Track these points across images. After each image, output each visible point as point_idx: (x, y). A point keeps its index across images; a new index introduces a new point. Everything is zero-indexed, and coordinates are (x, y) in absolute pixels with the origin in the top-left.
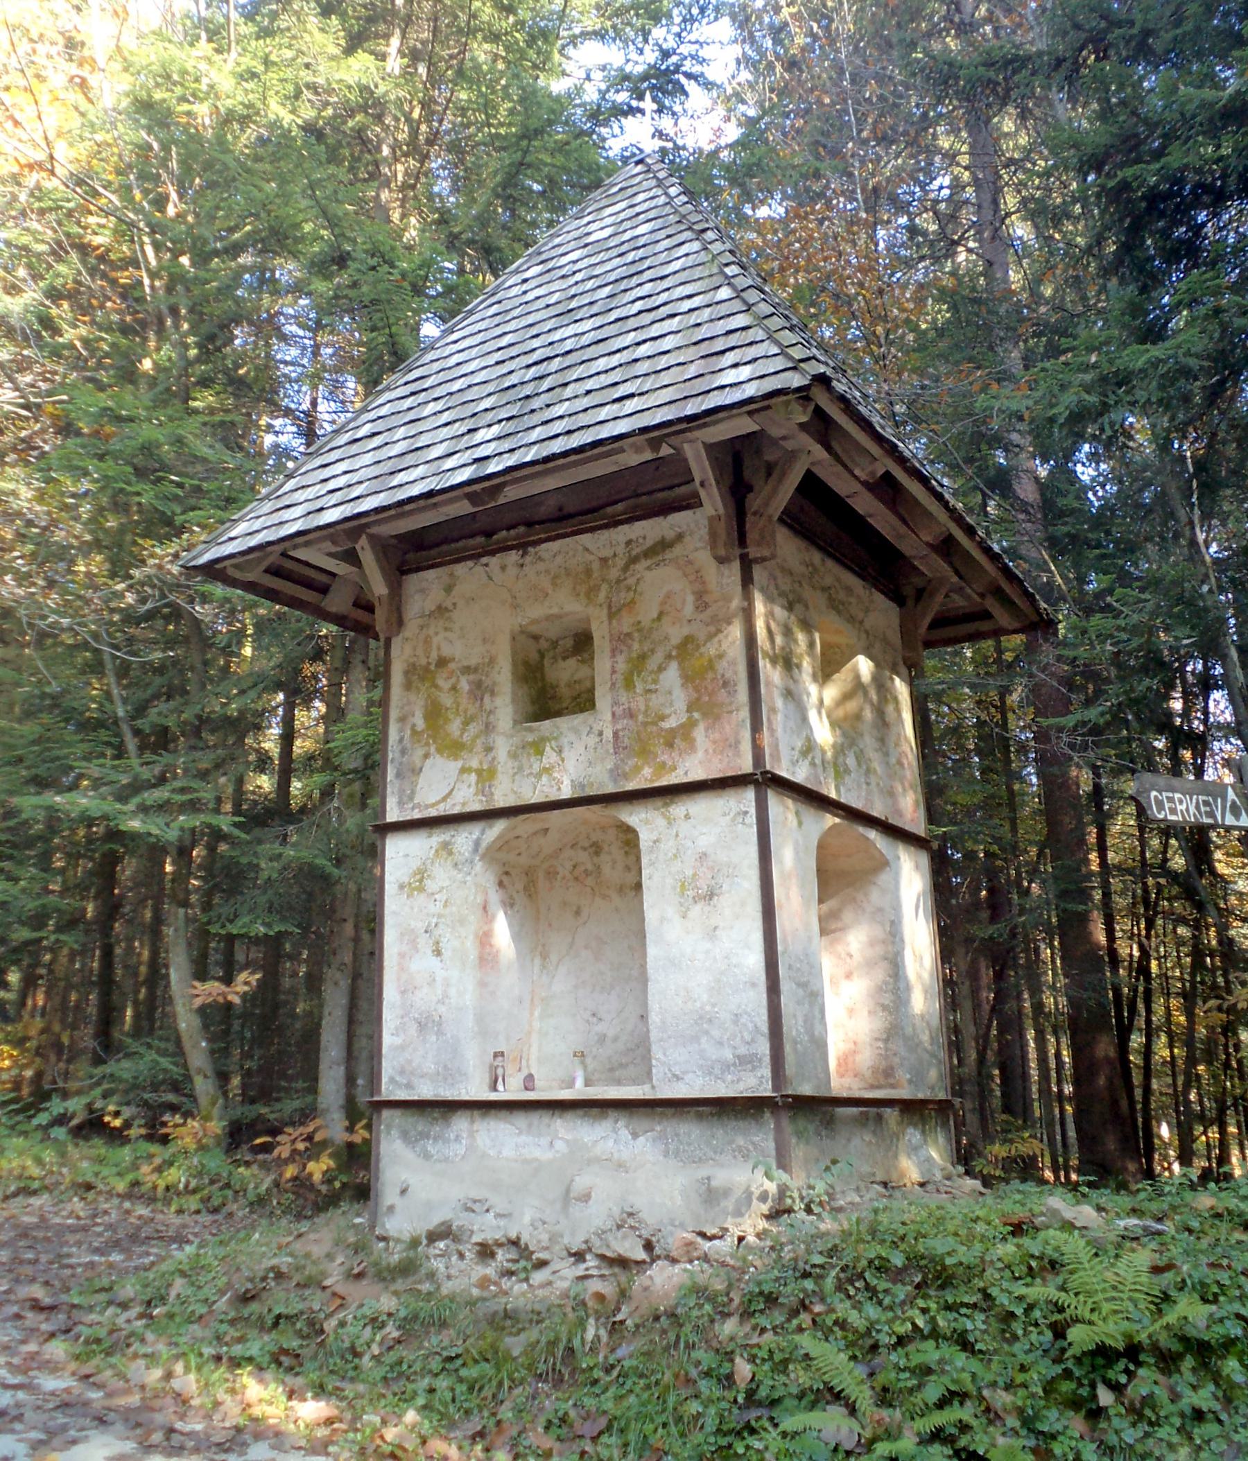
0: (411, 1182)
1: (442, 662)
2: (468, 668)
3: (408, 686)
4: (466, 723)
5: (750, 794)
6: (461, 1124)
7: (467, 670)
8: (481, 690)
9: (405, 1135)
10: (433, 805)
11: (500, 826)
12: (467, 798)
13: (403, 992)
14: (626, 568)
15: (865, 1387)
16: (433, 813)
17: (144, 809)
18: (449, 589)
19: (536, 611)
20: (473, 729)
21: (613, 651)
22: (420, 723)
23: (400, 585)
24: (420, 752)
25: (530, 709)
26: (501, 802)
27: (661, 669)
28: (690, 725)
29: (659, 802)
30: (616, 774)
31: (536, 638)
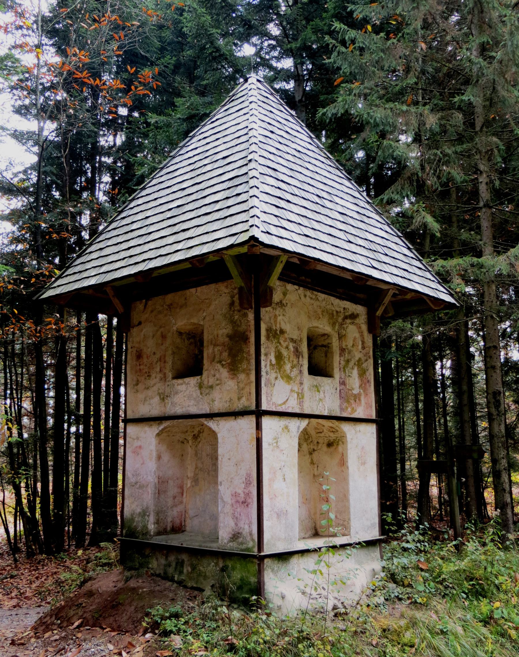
0: (284, 592)
1: (282, 332)
2: (292, 339)
3: (268, 338)
4: (292, 367)
7: (292, 340)
9: (273, 570)
10: (280, 405)
12: (293, 407)
13: (271, 499)
15: (85, 646)
19: (315, 324)
21: (340, 354)
22: (274, 361)
26: (307, 411)
27: (353, 369)
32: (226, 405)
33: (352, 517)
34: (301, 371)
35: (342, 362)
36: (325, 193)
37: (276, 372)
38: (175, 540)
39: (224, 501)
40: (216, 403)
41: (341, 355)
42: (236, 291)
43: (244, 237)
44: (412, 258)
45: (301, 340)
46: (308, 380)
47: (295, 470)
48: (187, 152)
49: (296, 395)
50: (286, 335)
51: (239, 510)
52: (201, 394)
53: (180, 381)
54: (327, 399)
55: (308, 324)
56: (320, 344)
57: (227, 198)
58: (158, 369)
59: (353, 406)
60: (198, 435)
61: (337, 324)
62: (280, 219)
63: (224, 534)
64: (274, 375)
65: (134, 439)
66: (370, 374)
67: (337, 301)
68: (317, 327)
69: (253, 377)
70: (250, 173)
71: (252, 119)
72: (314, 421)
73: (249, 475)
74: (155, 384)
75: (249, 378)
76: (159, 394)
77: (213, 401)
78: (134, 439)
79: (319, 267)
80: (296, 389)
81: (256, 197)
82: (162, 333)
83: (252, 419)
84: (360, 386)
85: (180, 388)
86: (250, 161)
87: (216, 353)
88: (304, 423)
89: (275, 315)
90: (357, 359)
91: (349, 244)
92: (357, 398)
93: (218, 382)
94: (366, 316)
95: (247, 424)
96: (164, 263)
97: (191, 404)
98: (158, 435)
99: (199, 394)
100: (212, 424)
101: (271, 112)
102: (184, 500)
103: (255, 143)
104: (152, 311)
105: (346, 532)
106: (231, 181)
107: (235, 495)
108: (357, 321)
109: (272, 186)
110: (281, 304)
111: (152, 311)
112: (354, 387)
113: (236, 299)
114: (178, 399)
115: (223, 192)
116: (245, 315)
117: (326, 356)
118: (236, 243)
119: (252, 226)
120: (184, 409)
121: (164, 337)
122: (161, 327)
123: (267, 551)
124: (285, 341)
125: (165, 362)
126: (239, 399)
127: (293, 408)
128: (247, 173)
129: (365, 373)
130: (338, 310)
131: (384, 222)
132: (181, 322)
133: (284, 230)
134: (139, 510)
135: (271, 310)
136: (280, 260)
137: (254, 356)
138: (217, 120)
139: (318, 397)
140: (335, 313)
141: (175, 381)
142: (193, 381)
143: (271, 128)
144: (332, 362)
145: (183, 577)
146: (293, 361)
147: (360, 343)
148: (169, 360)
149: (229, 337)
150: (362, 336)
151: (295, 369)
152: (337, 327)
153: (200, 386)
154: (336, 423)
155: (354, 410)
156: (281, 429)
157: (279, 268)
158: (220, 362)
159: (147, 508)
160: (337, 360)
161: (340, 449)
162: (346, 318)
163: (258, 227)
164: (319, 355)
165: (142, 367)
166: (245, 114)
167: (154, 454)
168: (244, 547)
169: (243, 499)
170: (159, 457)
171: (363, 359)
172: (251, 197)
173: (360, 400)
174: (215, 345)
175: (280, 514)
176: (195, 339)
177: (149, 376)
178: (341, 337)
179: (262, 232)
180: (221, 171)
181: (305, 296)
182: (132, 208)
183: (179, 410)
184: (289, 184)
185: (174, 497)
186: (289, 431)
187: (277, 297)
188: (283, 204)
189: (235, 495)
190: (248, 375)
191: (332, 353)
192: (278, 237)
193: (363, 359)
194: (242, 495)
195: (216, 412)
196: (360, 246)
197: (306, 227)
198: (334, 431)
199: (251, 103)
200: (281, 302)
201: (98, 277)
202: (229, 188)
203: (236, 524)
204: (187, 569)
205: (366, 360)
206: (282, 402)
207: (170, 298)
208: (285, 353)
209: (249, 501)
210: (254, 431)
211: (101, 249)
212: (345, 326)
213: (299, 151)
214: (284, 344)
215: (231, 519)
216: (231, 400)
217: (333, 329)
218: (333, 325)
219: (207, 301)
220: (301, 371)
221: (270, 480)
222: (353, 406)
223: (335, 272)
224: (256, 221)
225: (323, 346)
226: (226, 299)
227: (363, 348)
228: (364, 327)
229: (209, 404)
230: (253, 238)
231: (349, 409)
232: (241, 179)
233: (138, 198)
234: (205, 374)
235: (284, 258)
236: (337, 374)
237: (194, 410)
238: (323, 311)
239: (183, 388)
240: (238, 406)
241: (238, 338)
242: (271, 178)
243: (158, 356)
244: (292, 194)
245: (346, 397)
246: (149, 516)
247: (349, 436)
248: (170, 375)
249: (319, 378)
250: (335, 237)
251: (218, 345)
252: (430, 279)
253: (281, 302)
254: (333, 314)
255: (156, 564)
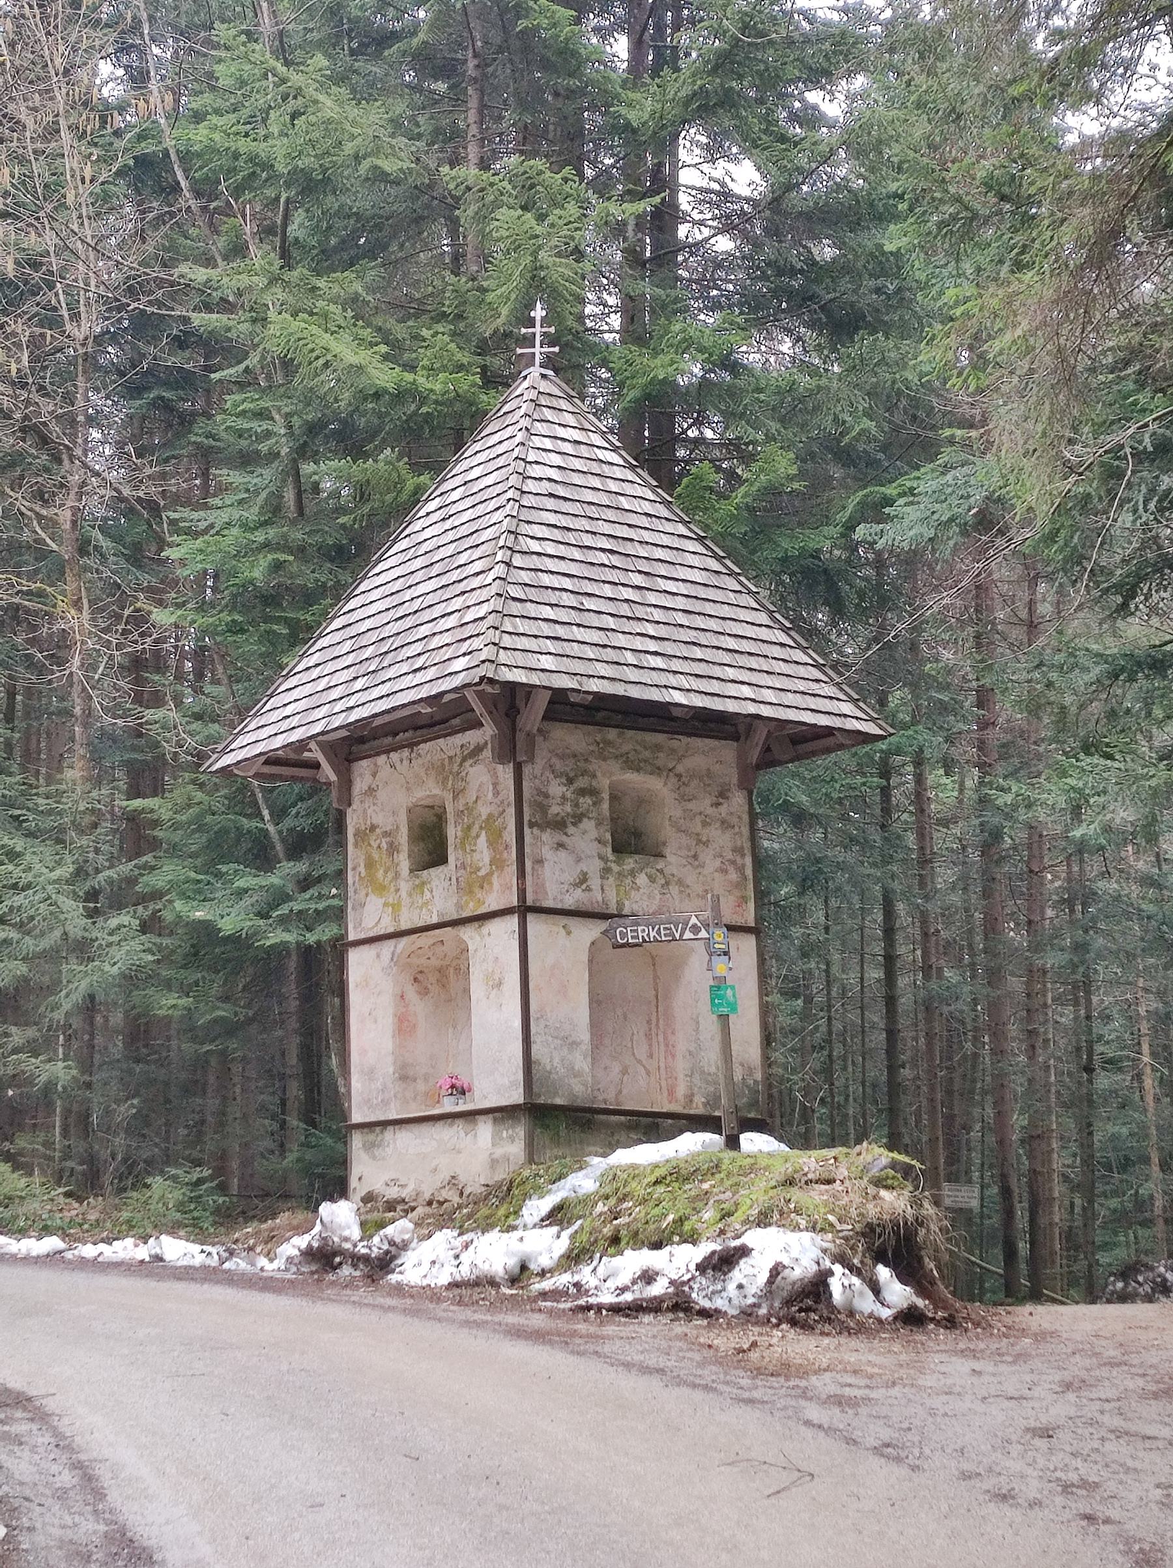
1: (373, 828)
3: (356, 845)
4: (386, 872)
5: (513, 922)
6: (389, 1134)
8: (393, 849)
11: (404, 942)
14: (461, 765)
16: (371, 934)
17: (283, 921)
18: (374, 775)
20: (390, 875)
23: (349, 770)
24: (364, 892)
25: (427, 858)
26: (405, 925)
27: (478, 836)
28: (490, 874)
29: (476, 924)
30: (459, 907)
31: (432, 807)
79: (378, 722)
155: (480, 902)
173: (491, 884)
214: (375, 845)
217: (444, 788)
245: (473, 883)
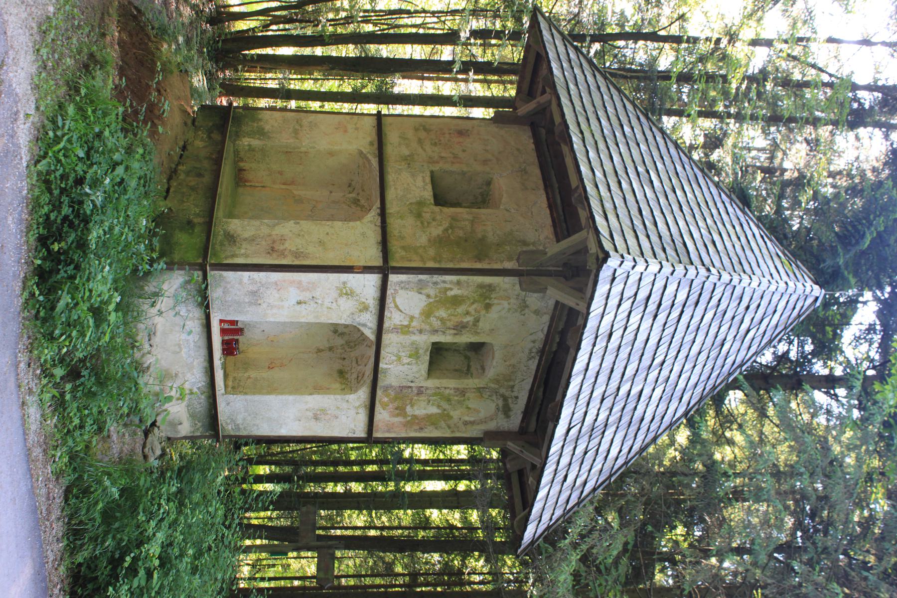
1: (488, 307)
2: (478, 321)
3: (481, 286)
4: (442, 320)
7: (477, 320)
9: (188, 282)
12: (393, 318)
13: (276, 283)
19: (498, 355)
21: (458, 389)
22: (450, 293)
26: (386, 338)
27: (439, 407)
32: (396, 233)
33: (249, 397)
34: (437, 331)
35: (447, 391)
36: (667, 373)
37: (436, 296)
38: (227, 171)
39: (274, 226)
40: (399, 221)
41: (456, 389)
42: (541, 248)
43: (607, 246)
44: (582, 492)
45: (477, 333)
46: (425, 340)
47: (311, 319)
48: (723, 203)
49: (406, 323)
50: (483, 312)
51: (264, 243)
52: (411, 204)
53: (428, 180)
54: (400, 368)
55: (497, 341)
56: (471, 363)
57: (660, 237)
58: (443, 155)
59: (391, 406)
60: (358, 205)
61: (497, 386)
62: (631, 300)
63: (235, 225)
64: (432, 292)
65: (356, 124)
66: (430, 432)
67: (528, 387)
68: (493, 358)
69: (431, 264)
70: (693, 267)
71: (765, 282)
72: (372, 352)
73: (306, 256)
74: (425, 150)
75: (429, 260)
76: (411, 155)
77: (402, 218)
78: (356, 124)
80: (414, 324)
81: (661, 269)
82: (490, 160)
83: (379, 262)
84: (415, 417)
85: (420, 179)
86: (708, 270)
87: (463, 223)
88: (371, 335)
89: (510, 298)
90: (452, 413)
91: (600, 397)
92: (400, 411)
93: (426, 224)
94: (506, 429)
95: (372, 255)
96: (578, 155)
97: (399, 191)
98: (361, 153)
99: (411, 201)
100: (373, 215)
101: (775, 311)
102: (277, 186)
103: (731, 280)
104: (518, 150)
105: (230, 389)
106: (682, 245)
107: (283, 240)
108: (501, 415)
109: (675, 296)
110: (524, 306)
111: (518, 150)
112: (415, 408)
113: (531, 248)
114: (406, 176)
115: (668, 233)
116: (510, 259)
117: (456, 370)
118: (602, 237)
119: (622, 256)
120: (392, 183)
121: (485, 162)
122: (498, 159)
123: (211, 274)
124: (475, 310)
125: (453, 163)
126: (403, 248)
127: (390, 318)
128: (692, 264)
129: (433, 424)
130: (516, 389)
131: (630, 456)
132: (503, 183)
133: (617, 303)
134: (267, 128)
135: (516, 293)
136: (579, 302)
137: (458, 266)
138: (765, 243)
139: (403, 354)
140: (511, 383)
141: (428, 174)
142: (428, 194)
143: (753, 307)
144: (447, 377)
145: (182, 176)
146: (450, 320)
147: (472, 419)
148: (455, 168)
149: (483, 239)
150: (481, 422)
151: (439, 323)
152: (493, 385)
153: (421, 203)
154: (368, 379)
156: (364, 300)
157: (570, 301)
158: (451, 227)
159: (269, 138)
160: (451, 383)
161: (337, 386)
162: (505, 399)
163: (620, 265)
164: (456, 361)
165: (447, 136)
166: (771, 275)
167: (336, 148)
168: (218, 247)
169: (276, 248)
170: (331, 154)
171: (451, 422)
172: (661, 263)
173: (397, 415)
174: (472, 222)
175: (255, 296)
176: (483, 199)
177: (435, 144)
178: (480, 390)
179: (615, 270)
180: (696, 235)
181: (534, 342)
182: (651, 130)
183: (390, 178)
184: (678, 321)
185: (281, 173)
186: (360, 311)
187: (534, 299)
188: (652, 307)
189: (283, 240)
190: (434, 260)
191: (460, 377)
192: (609, 293)
193: (451, 422)
194: (282, 248)
195: (388, 221)
196: (598, 415)
197: (622, 337)
198: (359, 379)
199: (786, 283)
200: (527, 306)
201: (562, 79)
202: (673, 241)
203: (245, 239)
204: (193, 181)
205: (449, 427)
206: (398, 304)
207: (536, 171)
208: (461, 309)
209: (275, 255)
210: (362, 263)
211: (599, 88)
212: (494, 398)
213: (723, 345)
214: (471, 309)
215: (252, 234)
216: (403, 238)
218: (497, 381)
219: (529, 214)
220: (437, 331)
221: (300, 282)
222: (391, 406)
223: (563, 382)
224: (628, 264)
225: (469, 367)
226: (531, 236)
227: (466, 423)
228: (492, 426)
229: (398, 213)
230: (607, 256)
231: (386, 399)
232: (684, 256)
233: (664, 139)
234: (437, 209)
235: (581, 307)
236: (431, 383)
237: (390, 195)
238: (514, 366)
239: (420, 183)
240: (395, 245)
241: (481, 248)
242: (685, 296)
243: (461, 155)
244: (665, 323)
245: (404, 395)
246: (260, 139)
247: (352, 397)
248: (436, 168)
249: (427, 358)
250: (609, 378)
251: (472, 225)
252: (553, 514)
253: (527, 306)
254: (510, 380)
255: (199, 143)
